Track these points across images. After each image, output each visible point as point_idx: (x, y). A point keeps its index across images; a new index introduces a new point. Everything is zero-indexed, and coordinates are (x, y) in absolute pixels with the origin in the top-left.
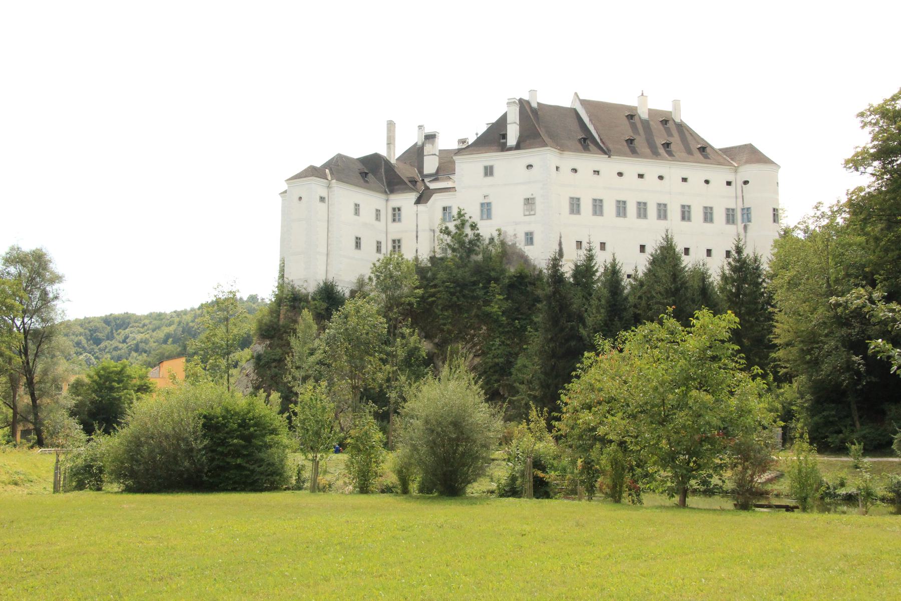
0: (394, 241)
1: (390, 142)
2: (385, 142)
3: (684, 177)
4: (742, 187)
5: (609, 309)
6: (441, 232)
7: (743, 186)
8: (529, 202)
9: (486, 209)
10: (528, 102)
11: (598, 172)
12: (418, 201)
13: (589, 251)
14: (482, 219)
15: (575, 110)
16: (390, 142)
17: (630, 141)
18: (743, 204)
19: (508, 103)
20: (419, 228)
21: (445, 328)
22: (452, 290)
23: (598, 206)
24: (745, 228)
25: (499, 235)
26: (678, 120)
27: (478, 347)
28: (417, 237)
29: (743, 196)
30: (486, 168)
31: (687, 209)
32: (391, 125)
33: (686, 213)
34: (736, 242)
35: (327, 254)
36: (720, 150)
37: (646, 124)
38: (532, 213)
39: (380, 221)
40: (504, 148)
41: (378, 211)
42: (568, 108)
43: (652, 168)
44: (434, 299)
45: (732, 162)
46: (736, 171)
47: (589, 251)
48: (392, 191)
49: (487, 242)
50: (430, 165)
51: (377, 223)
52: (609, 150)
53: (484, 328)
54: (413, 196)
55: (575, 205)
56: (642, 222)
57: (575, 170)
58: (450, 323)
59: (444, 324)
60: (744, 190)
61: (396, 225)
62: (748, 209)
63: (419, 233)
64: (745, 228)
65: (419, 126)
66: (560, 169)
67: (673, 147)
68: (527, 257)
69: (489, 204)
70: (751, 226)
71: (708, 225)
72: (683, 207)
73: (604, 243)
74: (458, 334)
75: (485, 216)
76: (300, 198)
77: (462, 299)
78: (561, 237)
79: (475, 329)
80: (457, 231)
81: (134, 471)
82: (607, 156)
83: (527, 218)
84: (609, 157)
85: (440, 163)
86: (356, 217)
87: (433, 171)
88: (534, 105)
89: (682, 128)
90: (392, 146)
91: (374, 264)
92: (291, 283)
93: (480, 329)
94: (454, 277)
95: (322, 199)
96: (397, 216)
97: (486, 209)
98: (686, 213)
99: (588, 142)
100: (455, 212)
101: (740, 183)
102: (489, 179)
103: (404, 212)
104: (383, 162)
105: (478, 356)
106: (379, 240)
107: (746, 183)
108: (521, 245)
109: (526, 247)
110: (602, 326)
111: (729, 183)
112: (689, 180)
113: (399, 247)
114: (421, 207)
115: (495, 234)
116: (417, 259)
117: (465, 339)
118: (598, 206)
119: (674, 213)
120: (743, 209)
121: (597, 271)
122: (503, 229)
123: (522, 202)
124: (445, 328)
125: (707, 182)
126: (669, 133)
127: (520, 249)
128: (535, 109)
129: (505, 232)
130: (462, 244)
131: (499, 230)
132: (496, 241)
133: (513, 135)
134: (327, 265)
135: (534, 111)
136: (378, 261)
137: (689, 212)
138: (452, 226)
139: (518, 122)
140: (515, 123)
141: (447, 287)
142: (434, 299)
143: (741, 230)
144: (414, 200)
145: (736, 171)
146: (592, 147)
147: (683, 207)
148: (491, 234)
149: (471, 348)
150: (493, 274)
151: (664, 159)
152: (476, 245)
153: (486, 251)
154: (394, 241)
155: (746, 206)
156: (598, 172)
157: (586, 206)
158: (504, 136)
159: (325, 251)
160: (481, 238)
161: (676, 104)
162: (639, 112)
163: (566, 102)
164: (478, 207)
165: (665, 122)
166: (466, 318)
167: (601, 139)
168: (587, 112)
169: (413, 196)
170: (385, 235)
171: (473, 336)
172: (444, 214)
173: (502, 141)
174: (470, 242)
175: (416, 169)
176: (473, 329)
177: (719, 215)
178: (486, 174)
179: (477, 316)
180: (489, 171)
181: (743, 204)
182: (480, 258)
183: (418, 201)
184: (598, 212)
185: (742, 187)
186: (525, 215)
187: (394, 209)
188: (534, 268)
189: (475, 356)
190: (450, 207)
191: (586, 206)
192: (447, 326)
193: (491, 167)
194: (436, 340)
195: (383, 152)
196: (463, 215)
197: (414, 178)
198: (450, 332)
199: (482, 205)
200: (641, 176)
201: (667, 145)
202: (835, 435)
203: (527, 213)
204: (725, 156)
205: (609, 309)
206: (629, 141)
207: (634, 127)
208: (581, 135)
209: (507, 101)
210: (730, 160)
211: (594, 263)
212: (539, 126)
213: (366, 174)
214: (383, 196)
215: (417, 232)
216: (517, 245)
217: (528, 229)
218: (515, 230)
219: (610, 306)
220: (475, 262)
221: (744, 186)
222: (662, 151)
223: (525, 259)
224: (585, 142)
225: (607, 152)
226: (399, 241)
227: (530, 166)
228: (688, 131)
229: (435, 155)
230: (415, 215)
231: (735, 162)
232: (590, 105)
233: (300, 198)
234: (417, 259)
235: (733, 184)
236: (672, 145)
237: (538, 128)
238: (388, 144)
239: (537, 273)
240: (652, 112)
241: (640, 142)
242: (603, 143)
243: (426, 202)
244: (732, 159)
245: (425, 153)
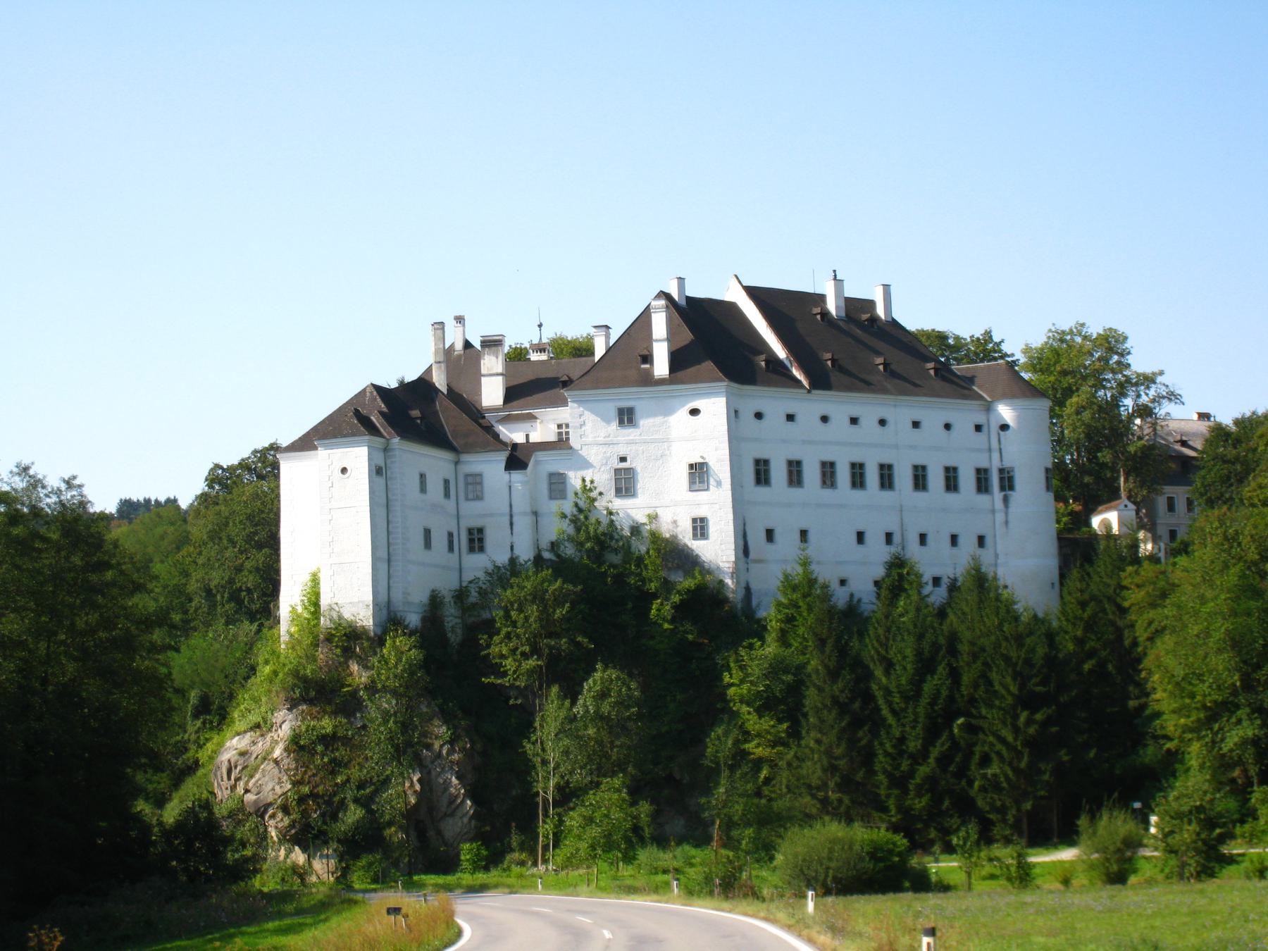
0: (470, 531)
4: (999, 434)
9: (625, 483)
18: (1001, 460)
20: (515, 510)
23: (795, 472)
24: (1006, 500)
29: (1000, 449)
40: (648, 380)
41: (446, 482)
43: (869, 407)
56: (858, 494)
60: (1002, 439)
63: (515, 519)
64: (1006, 500)
71: (951, 497)
72: (916, 468)
78: (744, 525)
101: (994, 428)
111: (978, 428)
118: (795, 472)
134: (389, 578)
147: (916, 468)
154: (470, 531)
158: (647, 358)
159: (385, 556)
181: (1001, 460)
184: (828, 482)
185: (999, 434)
191: (936, 479)
200: (790, 418)
215: (511, 516)
221: (1002, 433)
235: (985, 429)
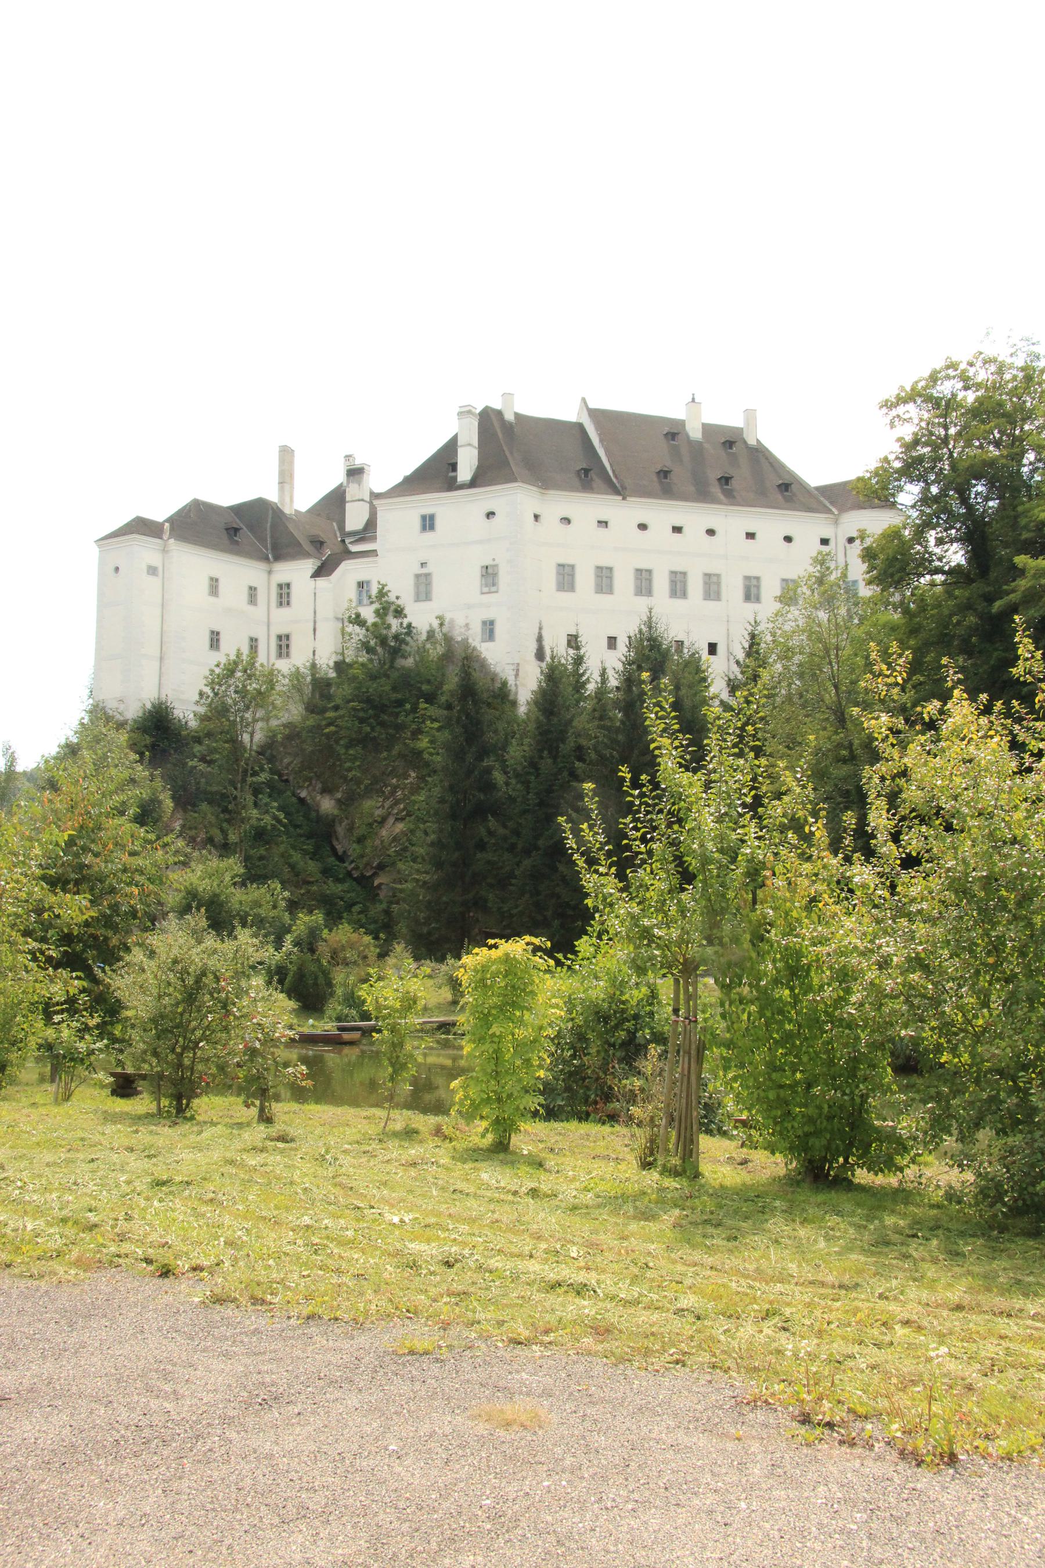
0: (280, 637)
1: (286, 478)
2: (277, 480)
3: (677, 525)
5: (539, 738)
6: (350, 622)
8: (489, 575)
9: (424, 586)
10: (499, 413)
11: (606, 523)
12: (318, 574)
14: (417, 599)
15: (580, 427)
16: (286, 478)
17: (664, 474)
19: (460, 414)
21: (350, 775)
22: (361, 714)
25: (441, 625)
26: (752, 442)
27: (402, 806)
28: (315, 630)
30: (424, 518)
31: (714, 579)
32: (286, 454)
33: (678, 586)
34: (750, 628)
35: (161, 659)
36: (817, 489)
37: (697, 449)
38: (493, 589)
39: (256, 605)
40: (452, 485)
41: (252, 590)
42: (570, 423)
44: (332, 728)
45: (831, 507)
46: (836, 522)
48: (278, 558)
49: (424, 637)
50: (355, 518)
51: (251, 608)
52: (624, 488)
53: (413, 774)
54: (309, 565)
55: (566, 578)
57: (567, 521)
58: (359, 766)
59: (350, 770)
60: (848, 552)
61: (284, 611)
65: (347, 456)
66: (542, 519)
67: (734, 483)
68: (484, 660)
69: (428, 575)
73: (615, 638)
74: (371, 784)
75: (423, 596)
76: (117, 569)
77: (378, 728)
78: (540, 629)
79: (398, 777)
80: (377, 620)
81: (353, 997)
82: (620, 498)
86: (212, 599)
87: (360, 526)
88: (509, 417)
89: (759, 456)
90: (287, 487)
91: (212, 671)
92: (101, 705)
93: (406, 776)
94: (364, 693)
95: (152, 571)
96: (285, 596)
98: (678, 586)
99: (592, 474)
100: (374, 591)
101: (842, 541)
102: (429, 535)
103: (294, 590)
104: (270, 512)
105: (402, 819)
106: (254, 636)
108: (476, 641)
109: (483, 644)
110: (525, 767)
112: (757, 536)
113: (288, 646)
114: (322, 582)
115: (436, 624)
116: (314, 666)
117: (383, 792)
119: (661, 584)
121: (588, 680)
122: (448, 617)
123: (477, 573)
124: (350, 775)
125: (788, 539)
126: (734, 459)
128: (510, 424)
129: (452, 621)
130: (383, 641)
131: (441, 618)
132: (439, 636)
133: (467, 465)
135: (508, 428)
136: (218, 666)
137: (758, 587)
138: (368, 614)
139: (476, 443)
140: (469, 445)
141: (354, 709)
142: (332, 728)
144: (311, 572)
145: (836, 522)
146: (598, 482)
148: (430, 625)
149: (392, 807)
150: (425, 687)
151: (718, 502)
152: (403, 641)
153: (422, 651)
154: (280, 637)
156: (606, 523)
157: (585, 579)
158: (454, 467)
160: (414, 631)
161: (750, 415)
162: (687, 428)
163: (569, 413)
164: (411, 581)
165: (729, 444)
166: (385, 759)
167: (614, 471)
168: (597, 429)
169: (309, 565)
170: (265, 628)
171: (395, 788)
172: (360, 594)
173: (452, 474)
174: (396, 637)
175: (335, 524)
176: (396, 776)
178: (424, 528)
179: (401, 756)
180: (428, 523)
182: (409, 662)
183: (318, 574)
186: (482, 593)
187: (280, 586)
188: (494, 677)
189: (397, 819)
190: (368, 582)
191: (585, 579)
192: (354, 773)
193: (432, 517)
194: (339, 795)
195: (272, 495)
196: (386, 594)
197: (318, 536)
198: (358, 782)
199: (417, 576)
201: (725, 480)
203: (486, 590)
204: (822, 499)
205: (539, 738)
206: (723, 481)
207: (675, 452)
209: (458, 410)
210: (828, 505)
212: (511, 453)
213: (236, 530)
214: (262, 566)
215: (315, 622)
216: (470, 641)
217: (488, 615)
218: (467, 617)
219: (540, 734)
220: (403, 668)
222: (716, 490)
224: (586, 475)
225: (618, 490)
226: (288, 637)
227: (490, 515)
228: (767, 459)
229: (363, 500)
231: (835, 507)
232: (600, 416)
233: (117, 569)
234: (314, 666)
236: (733, 482)
237: (507, 453)
238: (281, 483)
239: (498, 685)
240: (707, 428)
241: (680, 476)
242: (616, 477)
243: (329, 573)
244: (832, 503)
245: (347, 499)
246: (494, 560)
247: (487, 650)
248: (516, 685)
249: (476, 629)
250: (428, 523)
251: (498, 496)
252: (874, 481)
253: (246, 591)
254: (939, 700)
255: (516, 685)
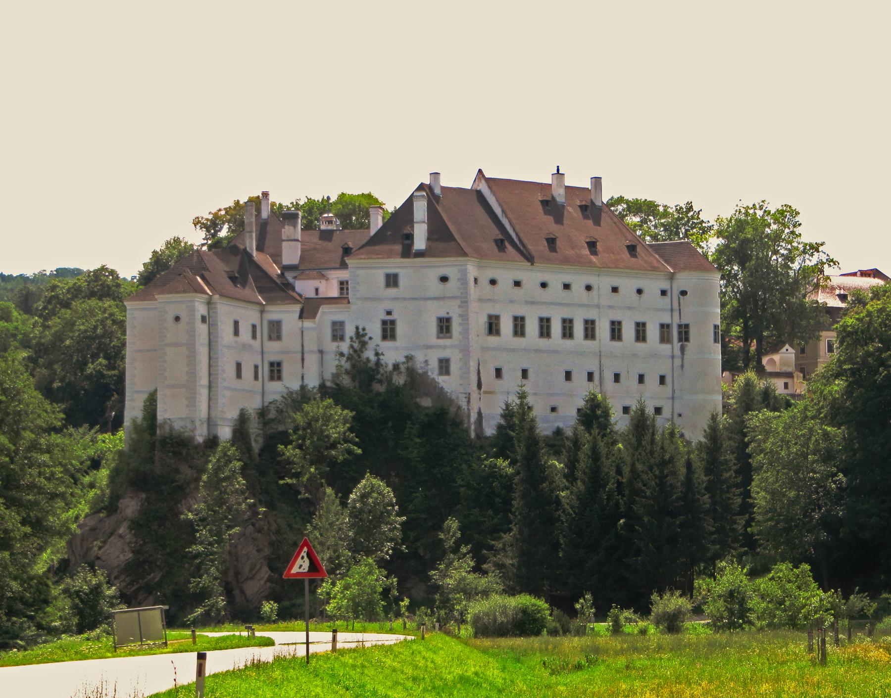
4: (679, 298)
7: (681, 297)
8: (444, 326)
9: (389, 330)
13: (521, 387)
20: (306, 349)
24: (682, 349)
28: (303, 359)
29: (680, 310)
40: (407, 252)
47: (521, 387)
49: (390, 367)
55: (493, 327)
56: (568, 342)
60: (681, 301)
62: (687, 326)
64: (682, 349)
68: (442, 388)
70: (690, 346)
82: (530, 264)
83: (441, 342)
84: (532, 264)
85: (303, 251)
97: (389, 330)
101: (676, 293)
107: (684, 293)
111: (664, 293)
120: (680, 326)
127: (434, 379)
143: (677, 352)
155: (684, 322)
158: (410, 237)
177: (653, 332)
185: (679, 298)
202: (695, 591)
208: (497, 234)
211: (683, 471)
215: (303, 354)
216: (430, 374)
223: (440, 394)
229: (297, 240)
230: (300, 333)
246: (448, 313)
247: (444, 381)
248: (468, 409)
249: (434, 365)
250: (392, 280)
251: (449, 266)
252: (848, 404)
253: (250, 328)
254: (461, 534)
255: (468, 409)
